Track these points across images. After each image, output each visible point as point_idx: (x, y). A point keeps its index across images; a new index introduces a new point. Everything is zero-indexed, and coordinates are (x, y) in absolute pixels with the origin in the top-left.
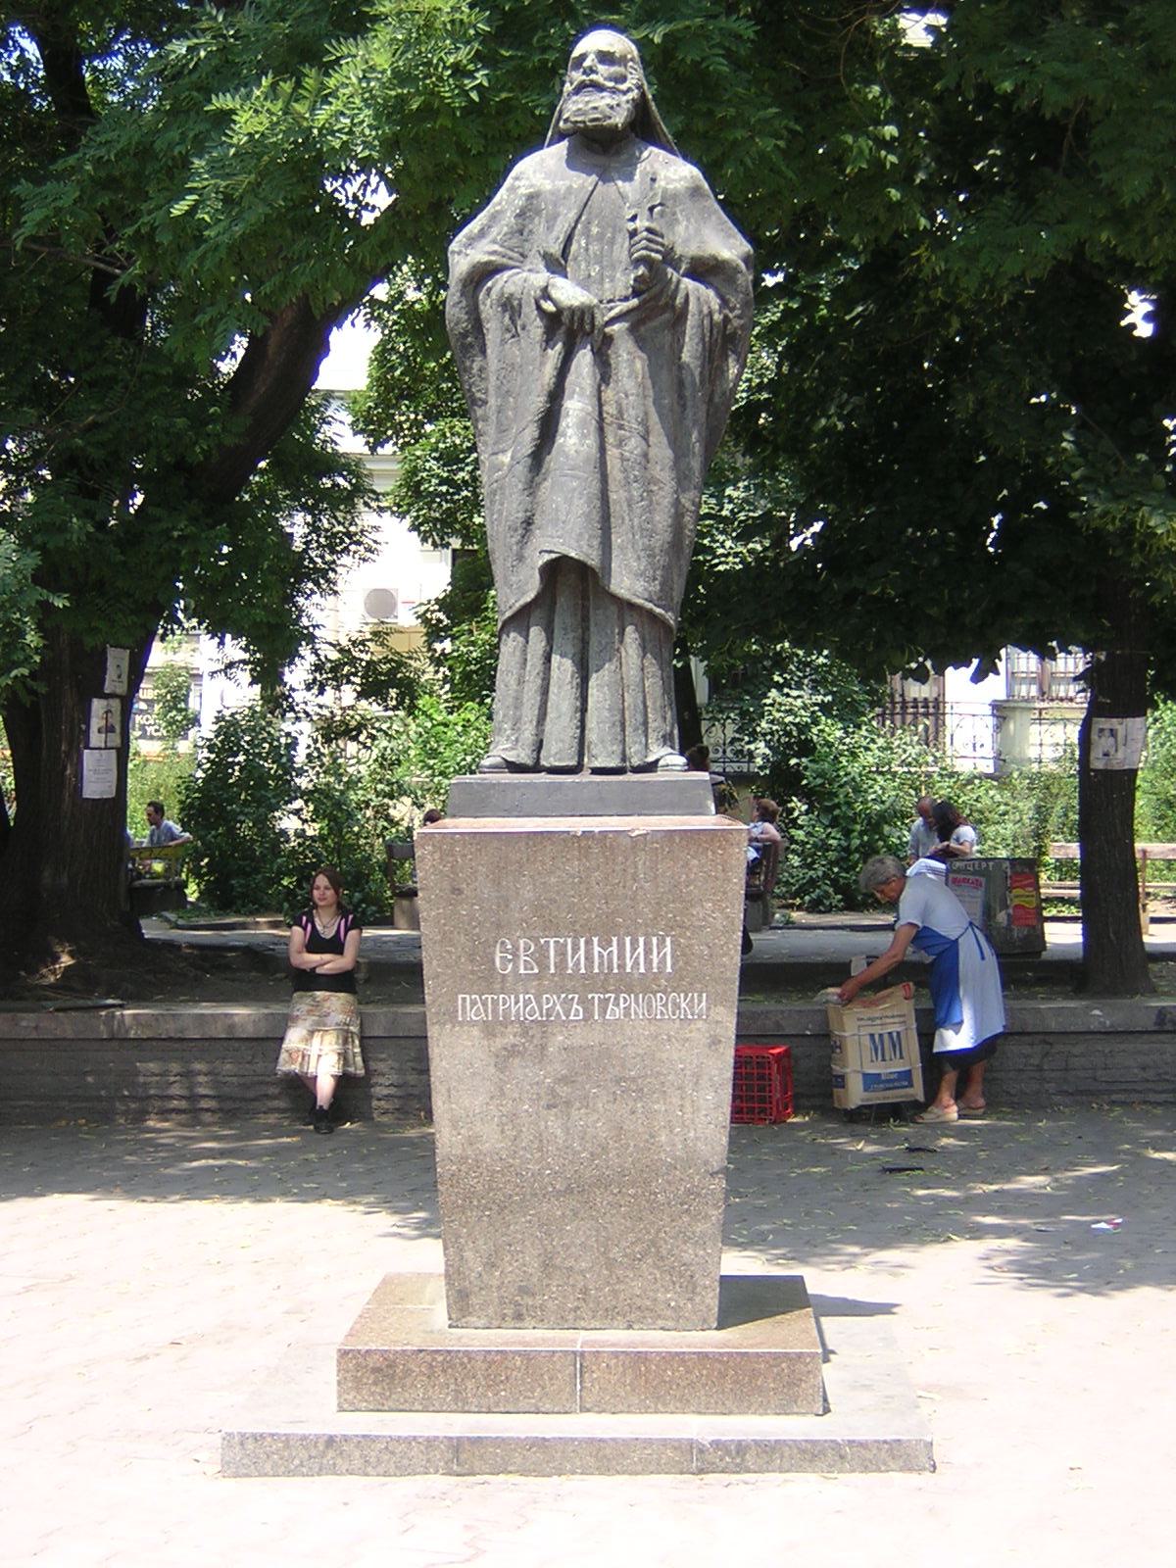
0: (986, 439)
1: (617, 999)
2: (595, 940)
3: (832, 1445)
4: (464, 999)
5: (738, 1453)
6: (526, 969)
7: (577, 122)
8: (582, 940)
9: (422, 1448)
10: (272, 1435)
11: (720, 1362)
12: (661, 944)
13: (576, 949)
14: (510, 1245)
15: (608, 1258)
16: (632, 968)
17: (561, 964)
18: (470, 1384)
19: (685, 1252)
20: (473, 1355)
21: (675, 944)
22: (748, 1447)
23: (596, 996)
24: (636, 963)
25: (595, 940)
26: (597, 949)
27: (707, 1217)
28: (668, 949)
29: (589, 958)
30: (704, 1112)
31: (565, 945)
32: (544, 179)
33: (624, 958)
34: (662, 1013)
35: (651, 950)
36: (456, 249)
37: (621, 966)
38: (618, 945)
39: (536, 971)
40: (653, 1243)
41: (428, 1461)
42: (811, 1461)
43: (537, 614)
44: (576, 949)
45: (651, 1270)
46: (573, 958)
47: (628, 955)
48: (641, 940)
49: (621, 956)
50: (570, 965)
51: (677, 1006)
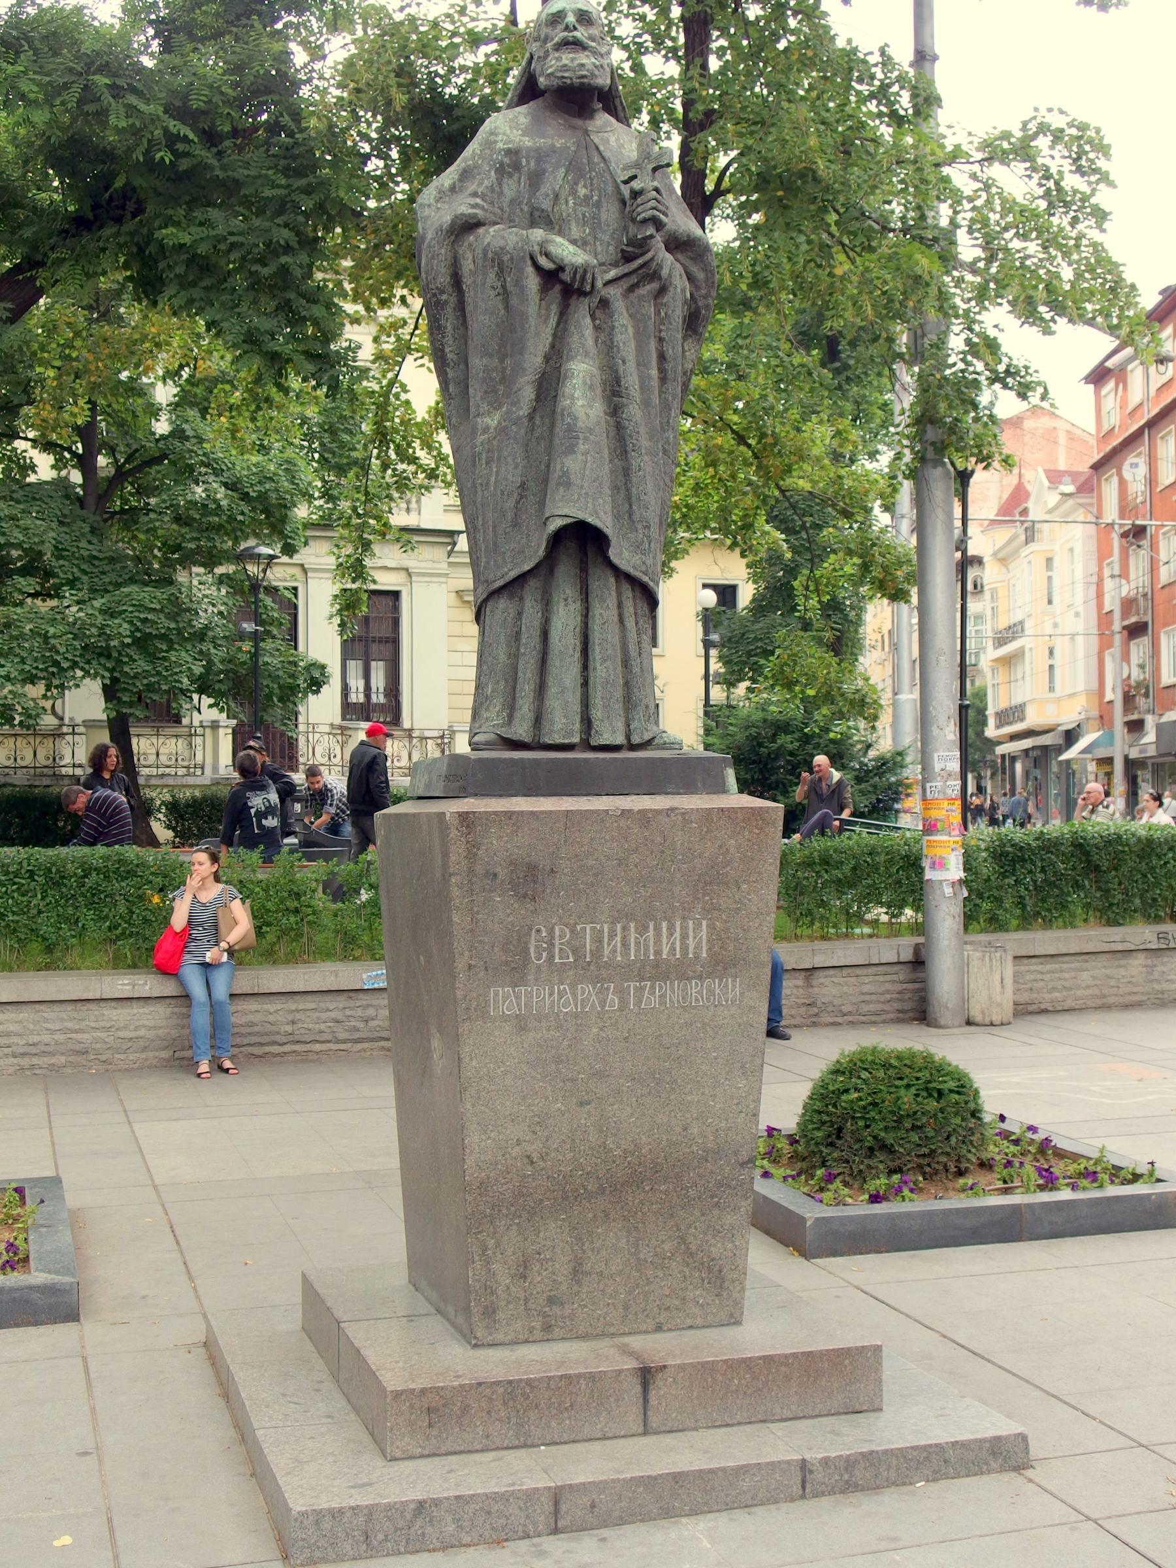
0: (914, 425)
1: (653, 987)
2: (632, 925)
3: (938, 1450)
4: (497, 994)
5: (846, 1469)
6: (561, 958)
7: (563, 77)
8: (619, 926)
9: (521, 1503)
10: (353, 1508)
11: (786, 1365)
12: (698, 926)
13: (612, 935)
14: (539, 1254)
15: (638, 1259)
16: (668, 955)
17: (597, 952)
18: (532, 1415)
19: (715, 1246)
20: (536, 1383)
21: (711, 927)
22: (856, 1461)
23: (632, 984)
24: (673, 949)
25: (632, 925)
26: (633, 936)
27: (736, 1209)
28: (704, 933)
29: (625, 945)
30: (736, 1101)
31: (601, 932)
32: (523, 135)
33: (661, 945)
34: (697, 1000)
35: (687, 934)
36: (426, 202)
37: (658, 953)
38: (655, 929)
39: (571, 960)
40: (683, 1240)
41: (527, 1517)
42: (917, 1469)
43: (533, 584)
44: (612, 935)
45: (681, 1268)
46: (609, 945)
47: (664, 941)
48: (678, 924)
49: (658, 941)
50: (606, 952)
51: (711, 992)
